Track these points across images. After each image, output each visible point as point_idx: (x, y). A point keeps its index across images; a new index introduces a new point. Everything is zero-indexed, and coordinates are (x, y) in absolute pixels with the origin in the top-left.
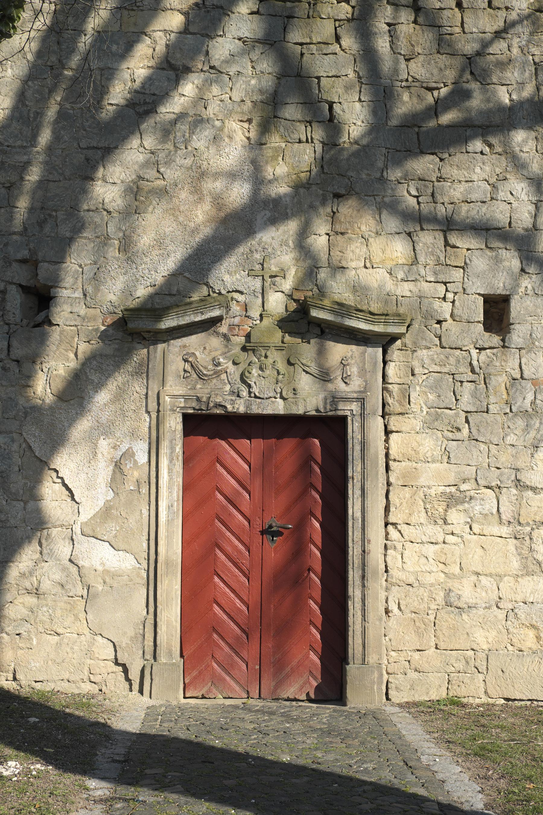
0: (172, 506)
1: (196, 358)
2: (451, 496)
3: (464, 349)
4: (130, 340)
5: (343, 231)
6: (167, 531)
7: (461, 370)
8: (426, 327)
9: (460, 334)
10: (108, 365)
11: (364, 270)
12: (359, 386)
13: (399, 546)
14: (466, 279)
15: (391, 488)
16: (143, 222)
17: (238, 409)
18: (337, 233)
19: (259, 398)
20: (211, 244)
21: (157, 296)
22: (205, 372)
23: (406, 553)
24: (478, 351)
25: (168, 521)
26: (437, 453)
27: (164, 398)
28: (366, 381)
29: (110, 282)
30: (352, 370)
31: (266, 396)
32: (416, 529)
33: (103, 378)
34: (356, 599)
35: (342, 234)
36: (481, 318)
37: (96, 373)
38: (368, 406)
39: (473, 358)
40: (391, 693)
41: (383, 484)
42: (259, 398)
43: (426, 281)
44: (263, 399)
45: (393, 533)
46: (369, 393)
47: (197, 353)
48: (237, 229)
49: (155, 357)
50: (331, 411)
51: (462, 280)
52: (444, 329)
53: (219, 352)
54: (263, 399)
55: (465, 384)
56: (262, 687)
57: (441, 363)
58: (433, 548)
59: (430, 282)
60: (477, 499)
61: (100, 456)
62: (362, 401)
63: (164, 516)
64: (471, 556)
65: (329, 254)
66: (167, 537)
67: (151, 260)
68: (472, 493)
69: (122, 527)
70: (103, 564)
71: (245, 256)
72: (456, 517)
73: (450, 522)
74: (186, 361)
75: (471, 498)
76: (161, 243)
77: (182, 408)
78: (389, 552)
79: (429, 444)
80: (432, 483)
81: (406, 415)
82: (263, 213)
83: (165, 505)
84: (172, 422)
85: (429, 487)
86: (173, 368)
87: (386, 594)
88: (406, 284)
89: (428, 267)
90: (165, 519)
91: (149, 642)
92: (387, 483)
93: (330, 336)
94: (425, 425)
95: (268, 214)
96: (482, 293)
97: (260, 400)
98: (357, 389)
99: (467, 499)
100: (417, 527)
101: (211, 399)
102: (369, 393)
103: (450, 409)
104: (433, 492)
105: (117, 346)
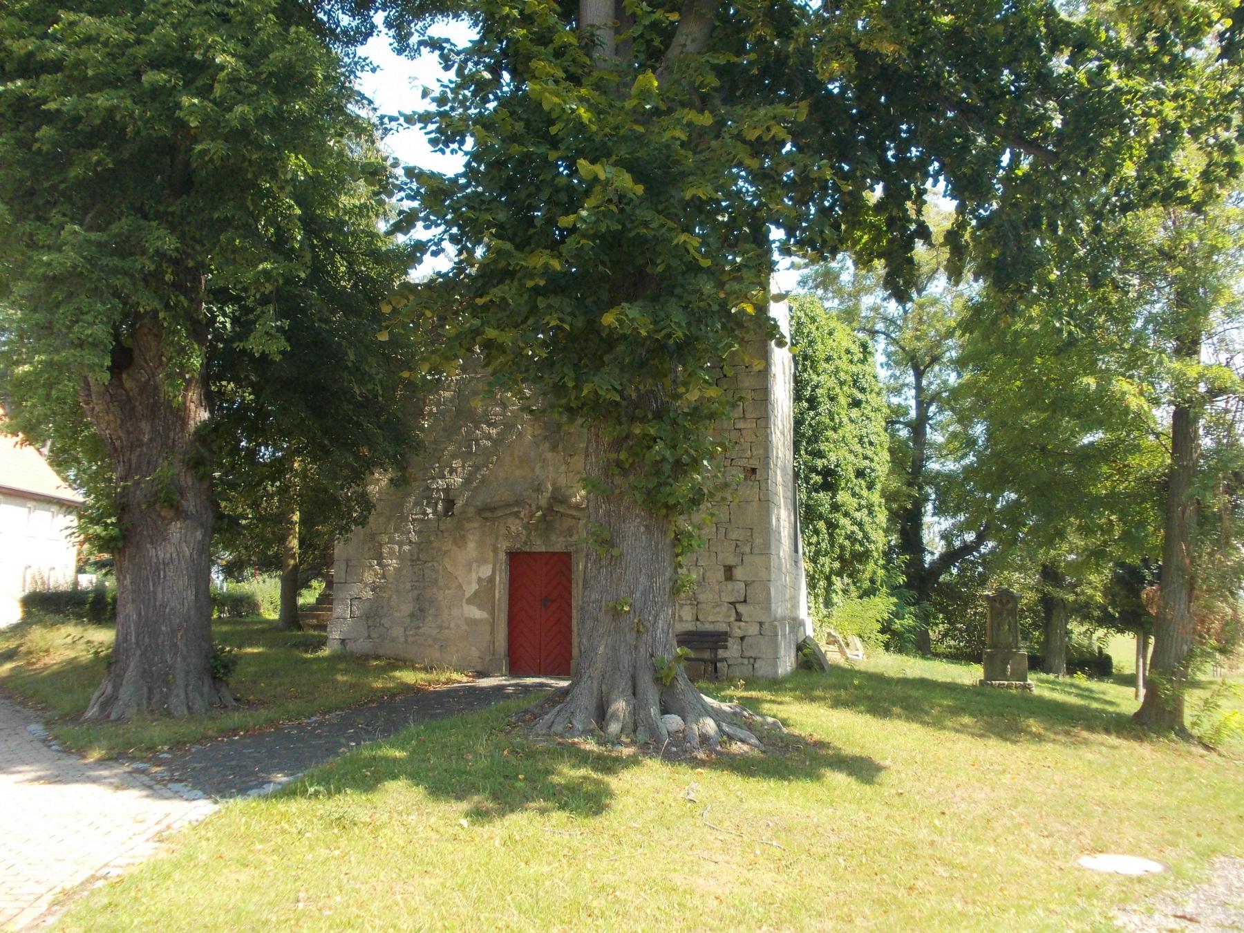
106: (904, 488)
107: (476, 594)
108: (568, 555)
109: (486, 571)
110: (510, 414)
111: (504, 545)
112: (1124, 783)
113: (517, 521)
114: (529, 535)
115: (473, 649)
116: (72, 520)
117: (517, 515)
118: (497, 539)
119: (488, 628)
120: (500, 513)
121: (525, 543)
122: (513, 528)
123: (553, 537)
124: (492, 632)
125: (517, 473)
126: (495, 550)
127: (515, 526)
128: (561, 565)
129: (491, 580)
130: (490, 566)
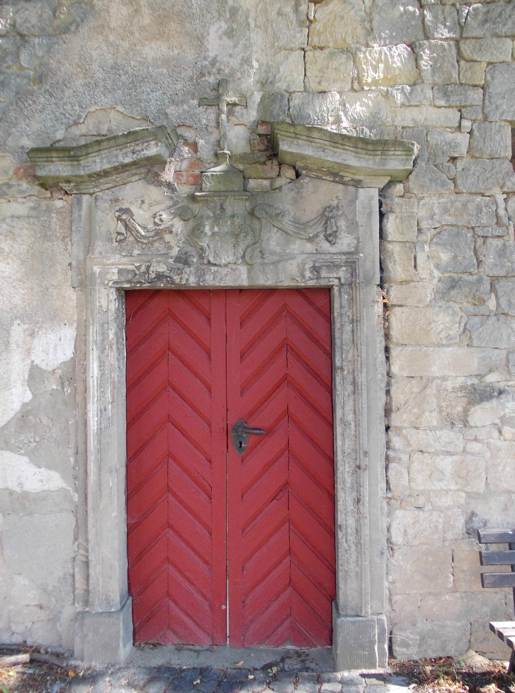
0: (105, 410)
1: (132, 215)
2: (474, 389)
3: (487, 194)
4: (49, 195)
5: (322, 45)
6: (99, 442)
7: (484, 221)
8: (436, 166)
9: (481, 174)
10: (21, 229)
11: (352, 94)
12: (349, 245)
13: (405, 457)
14: (487, 102)
15: (393, 381)
16: (64, 46)
17: (187, 280)
18: (315, 48)
19: (215, 265)
20: (151, 69)
21: (84, 138)
22: (143, 233)
23: (416, 466)
24: (505, 196)
25: (101, 429)
26: (455, 330)
27: (92, 269)
28: (358, 239)
29: (23, 123)
30: (339, 224)
31: (223, 262)
32: (427, 434)
33: (15, 246)
34: (349, 530)
35: (322, 48)
36: (509, 154)
37: (6, 240)
38: (360, 271)
39: (499, 205)
40: (396, 648)
41: (383, 375)
42: (215, 265)
43: (435, 106)
44: (220, 266)
45: (397, 442)
46: (361, 255)
47: (134, 209)
48: (184, 47)
49: (80, 216)
50: (312, 279)
51: (481, 103)
52: (459, 169)
53: (163, 206)
54: (220, 266)
55: (489, 240)
56: (229, 440)
57: (457, 213)
58: (449, 459)
59: (440, 107)
60: (509, 393)
61: (13, 346)
62: (352, 265)
63: (95, 424)
64: (501, 468)
65: (305, 75)
66: (99, 451)
67: (74, 92)
68: (502, 385)
69: (42, 438)
70: (21, 484)
71: (195, 81)
72: (482, 415)
73: (472, 424)
74: (119, 219)
75: (500, 393)
76: (87, 70)
77: (115, 283)
78: (392, 465)
79: (444, 322)
80: (447, 372)
81: (412, 284)
82: (217, 25)
83: (95, 408)
84: (102, 300)
85: (444, 379)
86: (103, 229)
87: (389, 520)
88: (407, 111)
89: (436, 88)
90: (96, 427)
91: (80, 584)
92: (388, 374)
93: (308, 179)
94: (437, 296)
95: (224, 26)
96: (509, 119)
97: (216, 268)
98: (345, 249)
99: (496, 394)
100: (428, 431)
101: (151, 268)
102: (361, 255)
103: (471, 274)
104: (449, 385)
105: (32, 204)
106: (209, 66)
107: (25, 415)
108: (318, 299)
109: (55, 348)
110: (81, 610)
111: (113, 267)
112: (156, 83)
113: (155, 193)
114: (196, 232)
115: (22, 581)
116: (365, 31)
117: (150, 169)
118: (89, 249)
119: (68, 521)
120: (98, 163)
121: (183, 260)
122: (141, 216)
123: (273, 241)
124: (81, 529)
125: (153, 50)
126: (85, 284)
127: (148, 205)
128: (301, 328)
129: (73, 373)
130: (69, 333)
